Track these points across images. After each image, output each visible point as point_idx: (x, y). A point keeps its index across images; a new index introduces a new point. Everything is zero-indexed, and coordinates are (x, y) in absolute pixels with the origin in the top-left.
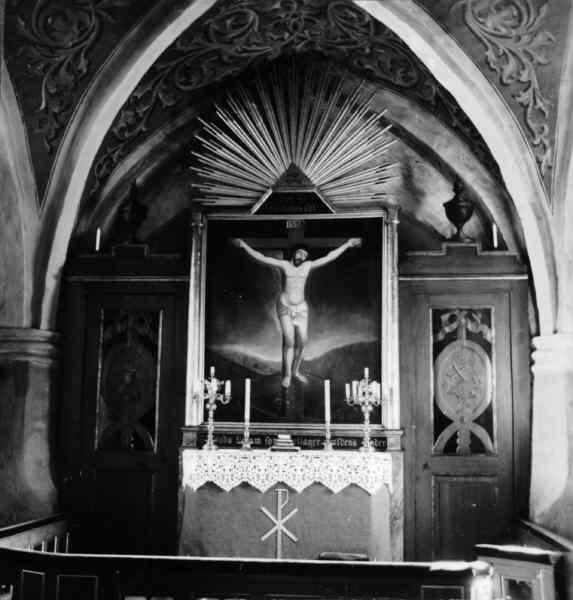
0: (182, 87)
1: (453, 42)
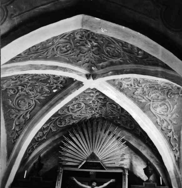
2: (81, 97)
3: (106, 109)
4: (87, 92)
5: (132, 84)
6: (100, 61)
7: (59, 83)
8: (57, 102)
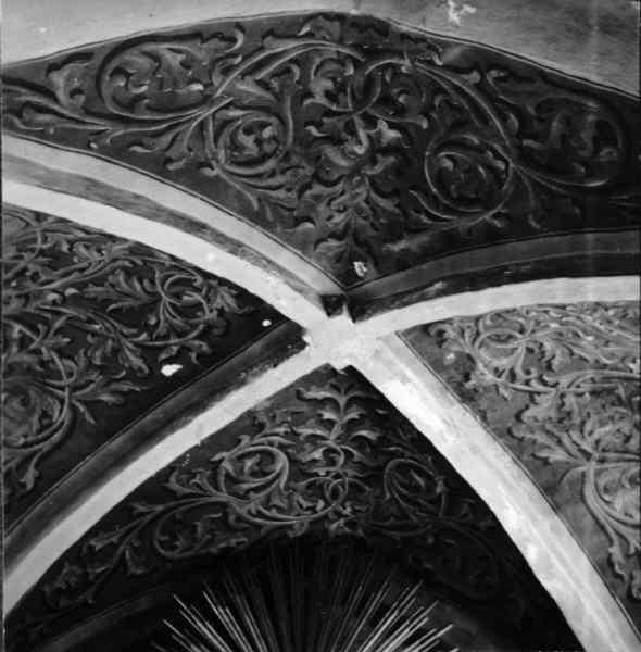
0: (162, 551)
1: (563, 528)
2: (278, 421)
3: (378, 497)
4: (312, 394)
5: (519, 371)
6: (395, 231)
7: (194, 334)
8: (170, 423)
